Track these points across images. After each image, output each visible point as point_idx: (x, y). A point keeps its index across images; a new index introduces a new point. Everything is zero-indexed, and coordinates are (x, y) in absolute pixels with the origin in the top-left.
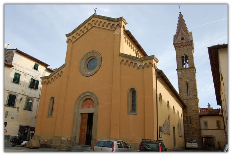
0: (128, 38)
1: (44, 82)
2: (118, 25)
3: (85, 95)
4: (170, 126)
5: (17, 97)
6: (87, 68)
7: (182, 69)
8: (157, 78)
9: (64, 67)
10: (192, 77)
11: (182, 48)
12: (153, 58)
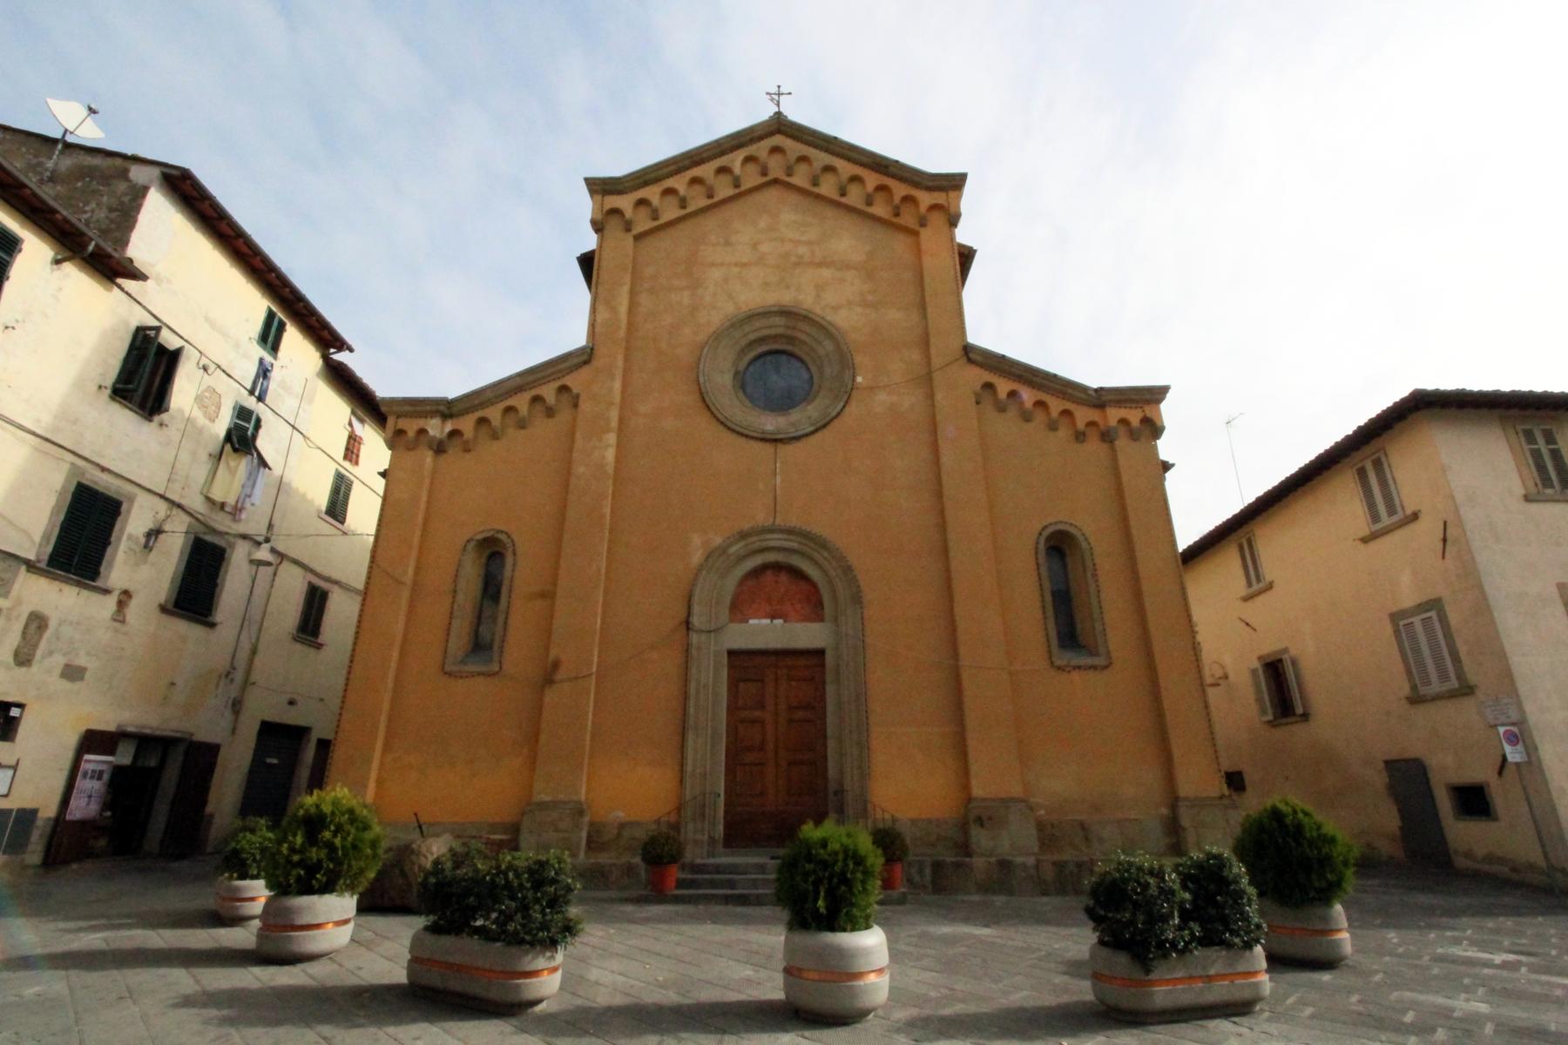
3: (757, 545)
5: (129, 512)
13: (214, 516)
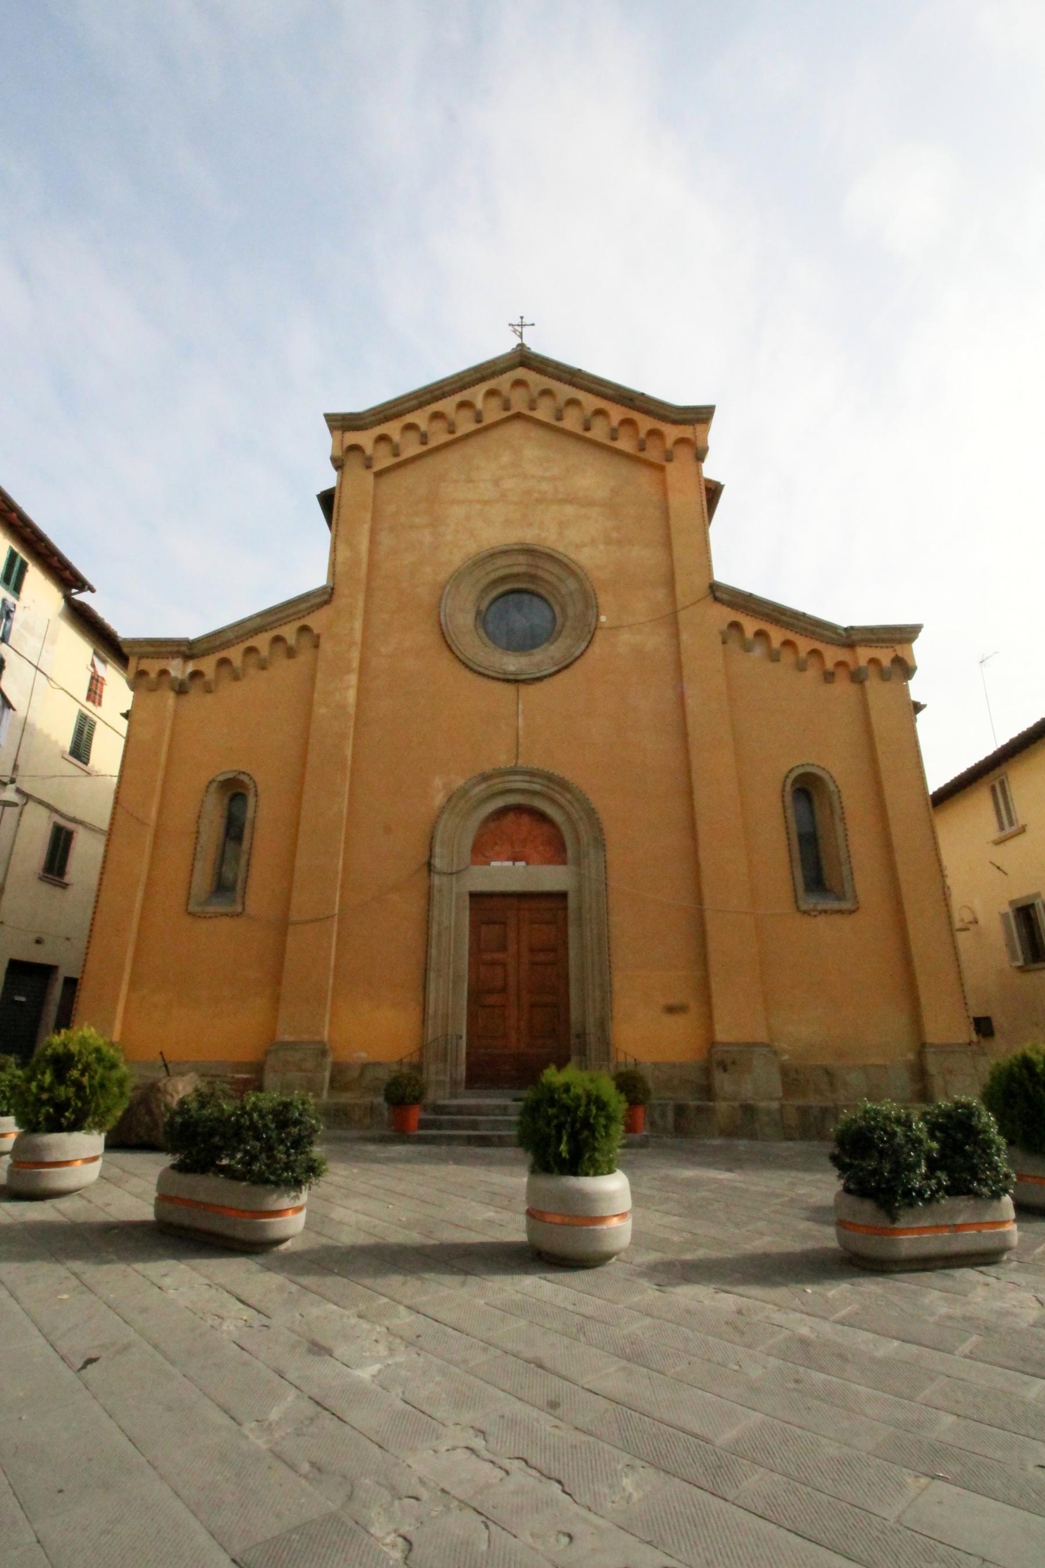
9: (327, 602)
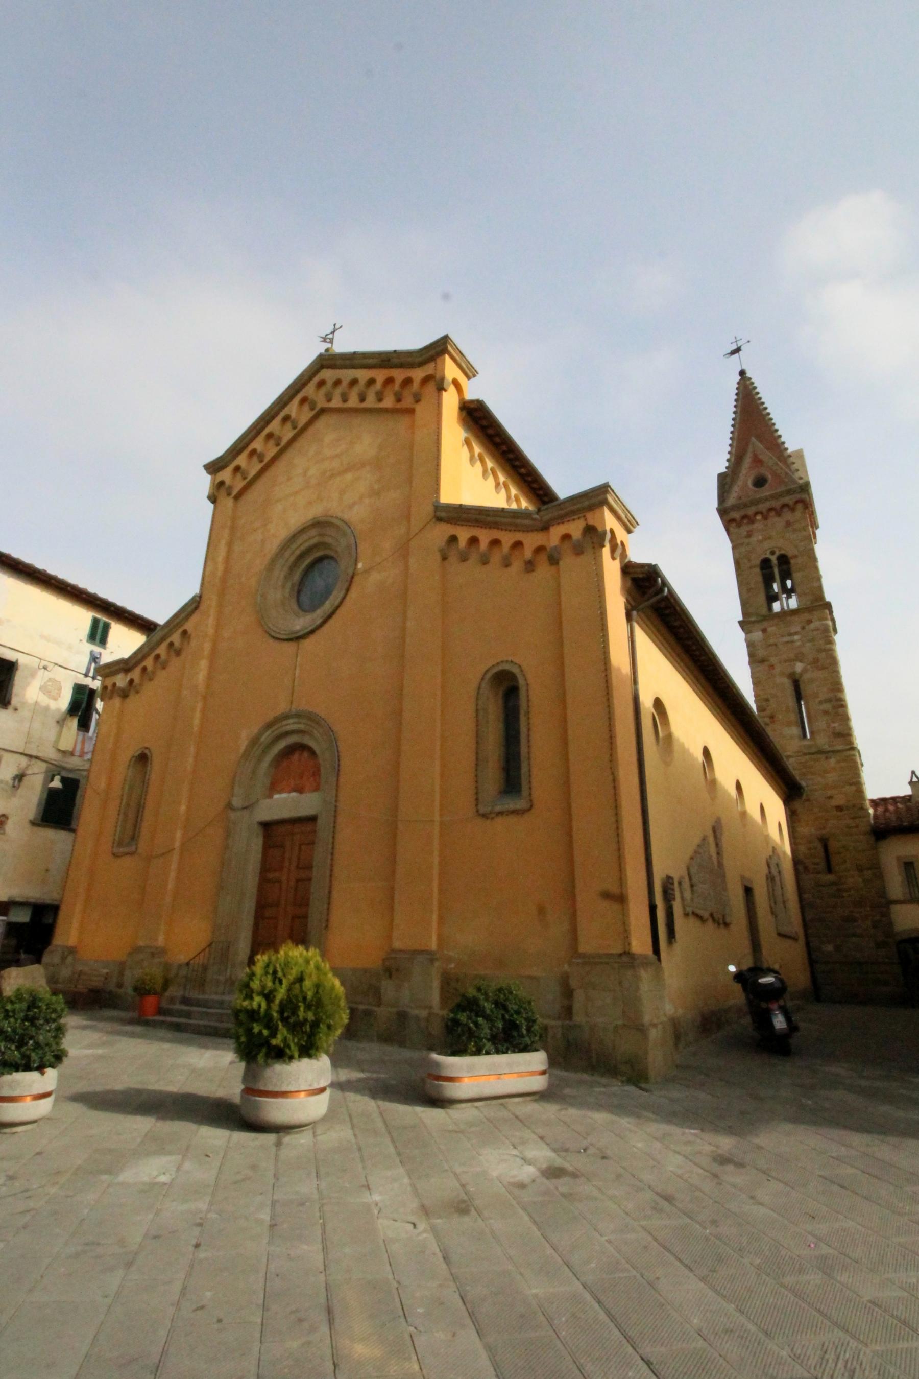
0: (487, 449)
1: (110, 688)
2: (427, 380)
4: (724, 876)
6: (294, 600)
7: (765, 618)
8: (634, 613)
9: (196, 608)
10: (820, 651)
11: (758, 525)
12: (600, 498)
13: (66, 760)
